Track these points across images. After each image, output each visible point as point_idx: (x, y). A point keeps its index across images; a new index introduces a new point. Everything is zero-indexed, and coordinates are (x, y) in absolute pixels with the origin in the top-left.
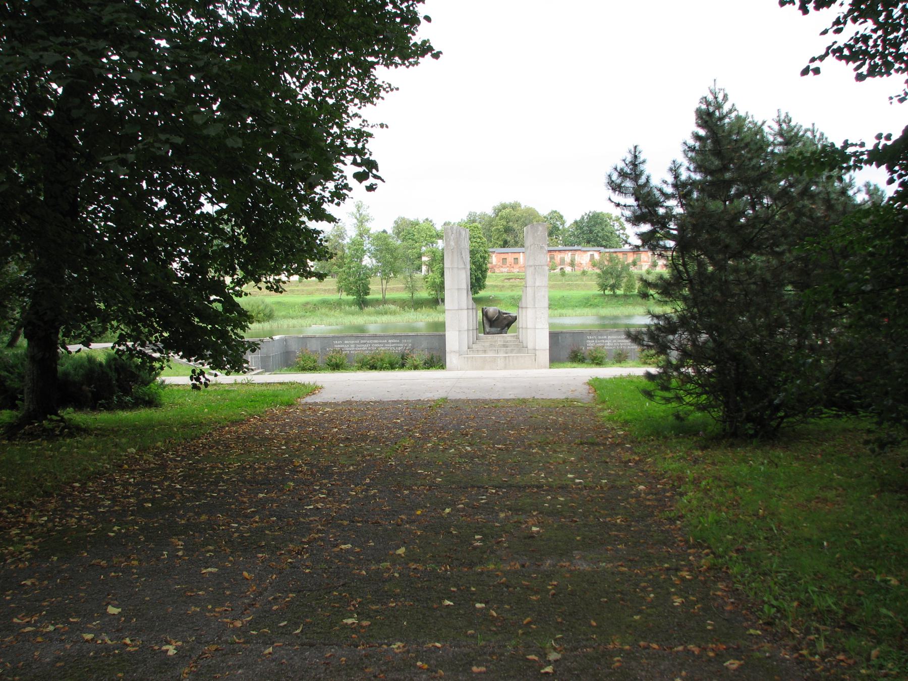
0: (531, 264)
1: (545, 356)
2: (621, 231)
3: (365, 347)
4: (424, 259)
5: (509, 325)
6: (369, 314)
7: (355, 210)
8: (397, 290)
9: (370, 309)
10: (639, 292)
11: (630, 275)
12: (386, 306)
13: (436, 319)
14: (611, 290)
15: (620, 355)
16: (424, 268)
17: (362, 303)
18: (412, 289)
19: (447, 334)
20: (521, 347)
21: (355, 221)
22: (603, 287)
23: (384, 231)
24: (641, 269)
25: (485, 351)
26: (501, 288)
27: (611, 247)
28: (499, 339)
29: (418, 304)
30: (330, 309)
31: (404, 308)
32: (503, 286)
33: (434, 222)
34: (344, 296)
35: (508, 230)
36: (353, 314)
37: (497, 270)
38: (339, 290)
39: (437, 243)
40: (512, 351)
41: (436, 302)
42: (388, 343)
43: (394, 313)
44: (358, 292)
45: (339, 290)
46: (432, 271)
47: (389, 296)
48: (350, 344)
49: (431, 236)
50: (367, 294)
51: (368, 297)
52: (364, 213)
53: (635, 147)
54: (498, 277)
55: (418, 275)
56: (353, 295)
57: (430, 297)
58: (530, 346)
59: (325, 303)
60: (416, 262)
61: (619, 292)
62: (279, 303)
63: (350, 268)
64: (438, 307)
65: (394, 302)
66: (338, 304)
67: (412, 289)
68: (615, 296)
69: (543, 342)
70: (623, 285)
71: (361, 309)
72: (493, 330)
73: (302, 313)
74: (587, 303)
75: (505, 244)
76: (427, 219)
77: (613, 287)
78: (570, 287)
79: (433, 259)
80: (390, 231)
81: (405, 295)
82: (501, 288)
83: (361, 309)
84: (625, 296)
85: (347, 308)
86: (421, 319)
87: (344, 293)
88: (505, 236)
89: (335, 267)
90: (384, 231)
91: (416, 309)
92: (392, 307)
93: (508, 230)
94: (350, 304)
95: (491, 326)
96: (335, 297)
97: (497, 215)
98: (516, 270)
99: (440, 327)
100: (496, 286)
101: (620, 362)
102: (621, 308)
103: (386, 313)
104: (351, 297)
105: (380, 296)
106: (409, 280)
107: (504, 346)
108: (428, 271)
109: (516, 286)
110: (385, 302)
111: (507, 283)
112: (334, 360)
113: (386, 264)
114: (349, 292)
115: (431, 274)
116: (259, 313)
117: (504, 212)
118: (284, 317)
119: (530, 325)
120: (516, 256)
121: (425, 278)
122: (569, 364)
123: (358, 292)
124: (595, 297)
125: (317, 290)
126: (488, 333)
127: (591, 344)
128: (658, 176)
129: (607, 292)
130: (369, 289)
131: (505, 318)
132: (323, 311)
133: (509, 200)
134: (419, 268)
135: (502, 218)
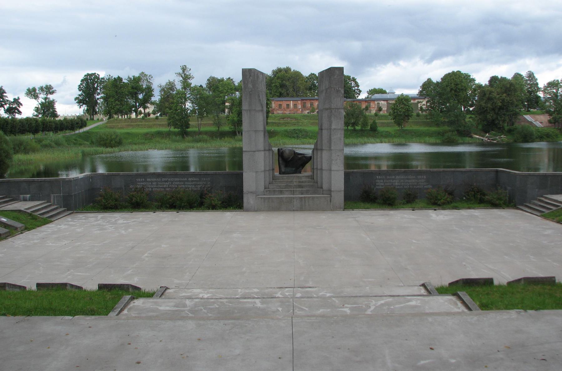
0: (327, 107)
1: (339, 198)
2: (356, 88)
3: (166, 185)
4: (227, 104)
5: (303, 165)
6: (189, 142)
7: (181, 71)
8: (209, 125)
9: (190, 138)
10: (371, 128)
11: (365, 117)
12: (201, 136)
13: (234, 146)
14: (352, 126)
15: (408, 195)
16: (226, 110)
17: (184, 134)
18: (218, 124)
19: (245, 175)
20: (316, 186)
21: (181, 79)
22: (347, 124)
23: (201, 86)
24: (370, 112)
25: (281, 192)
27: (350, 98)
28: (294, 178)
29: (222, 135)
30: (163, 137)
31: (212, 137)
32: (279, 123)
33: (234, 80)
34: (172, 129)
35: (282, 86)
36: (177, 141)
37: (275, 112)
38: (169, 125)
39: (235, 94)
40: (307, 192)
41: (235, 132)
42: (188, 181)
43: (205, 141)
44: (182, 126)
45: (169, 125)
46: (232, 113)
47: (203, 129)
48: (152, 182)
49: (231, 89)
50: (188, 127)
51: (189, 130)
52: (187, 73)
54: (276, 117)
55: (222, 115)
56: (178, 128)
57: (231, 130)
58: (325, 186)
59: (159, 134)
60: (221, 106)
61: (358, 128)
62: (128, 133)
63: (176, 110)
64: (236, 137)
65: (206, 133)
67: (218, 124)
68: (355, 130)
69: (337, 180)
70: (360, 123)
71: (183, 137)
72: (289, 169)
73: (143, 141)
75: (281, 95)
76: (229, 78)
77: (354, 124)
79: (232, 105)
80: (204, 86)
81: (214, 129)
82: (278, 124)
83: (183, 137)
84: (361, 130)
85: (174, 137)
86: (224, 146)
87: (172, 127)
88: (280, 90)
89: (167, 109)
90: (201, 86)
91: (221, 139)
92: (205, 137)
93: (282, 86)
95: (286, 166)
97: (275, 76)
99: (237, 157)
100: (275, 123)
102: (359, 139)
103: (200, 141)
104: (176, 130)
105: (197, 129)
106: (216, 118)
107: (300, 186)
108: (229, 113)
109: (288, 123)
110: (200, 133)
111: (282, 121)
112: (134, 199)
113: (201, 108)
114: (175, 126)
115: (231, 114)
116: (111, 141)
117: (279, 75)
118: (130, 143)
119: (325, 166)
120: (288, 103)
121: (227, 117)
122: (362, 204)
123: (182, 126)
125: (155, 125)
126: (284, 173)
127: (380, 184)
129: (349, 128)
130: (189, 124)
131: (300, 159)
132: (157, 139)
134: (224, 111)
135: (278, 78)
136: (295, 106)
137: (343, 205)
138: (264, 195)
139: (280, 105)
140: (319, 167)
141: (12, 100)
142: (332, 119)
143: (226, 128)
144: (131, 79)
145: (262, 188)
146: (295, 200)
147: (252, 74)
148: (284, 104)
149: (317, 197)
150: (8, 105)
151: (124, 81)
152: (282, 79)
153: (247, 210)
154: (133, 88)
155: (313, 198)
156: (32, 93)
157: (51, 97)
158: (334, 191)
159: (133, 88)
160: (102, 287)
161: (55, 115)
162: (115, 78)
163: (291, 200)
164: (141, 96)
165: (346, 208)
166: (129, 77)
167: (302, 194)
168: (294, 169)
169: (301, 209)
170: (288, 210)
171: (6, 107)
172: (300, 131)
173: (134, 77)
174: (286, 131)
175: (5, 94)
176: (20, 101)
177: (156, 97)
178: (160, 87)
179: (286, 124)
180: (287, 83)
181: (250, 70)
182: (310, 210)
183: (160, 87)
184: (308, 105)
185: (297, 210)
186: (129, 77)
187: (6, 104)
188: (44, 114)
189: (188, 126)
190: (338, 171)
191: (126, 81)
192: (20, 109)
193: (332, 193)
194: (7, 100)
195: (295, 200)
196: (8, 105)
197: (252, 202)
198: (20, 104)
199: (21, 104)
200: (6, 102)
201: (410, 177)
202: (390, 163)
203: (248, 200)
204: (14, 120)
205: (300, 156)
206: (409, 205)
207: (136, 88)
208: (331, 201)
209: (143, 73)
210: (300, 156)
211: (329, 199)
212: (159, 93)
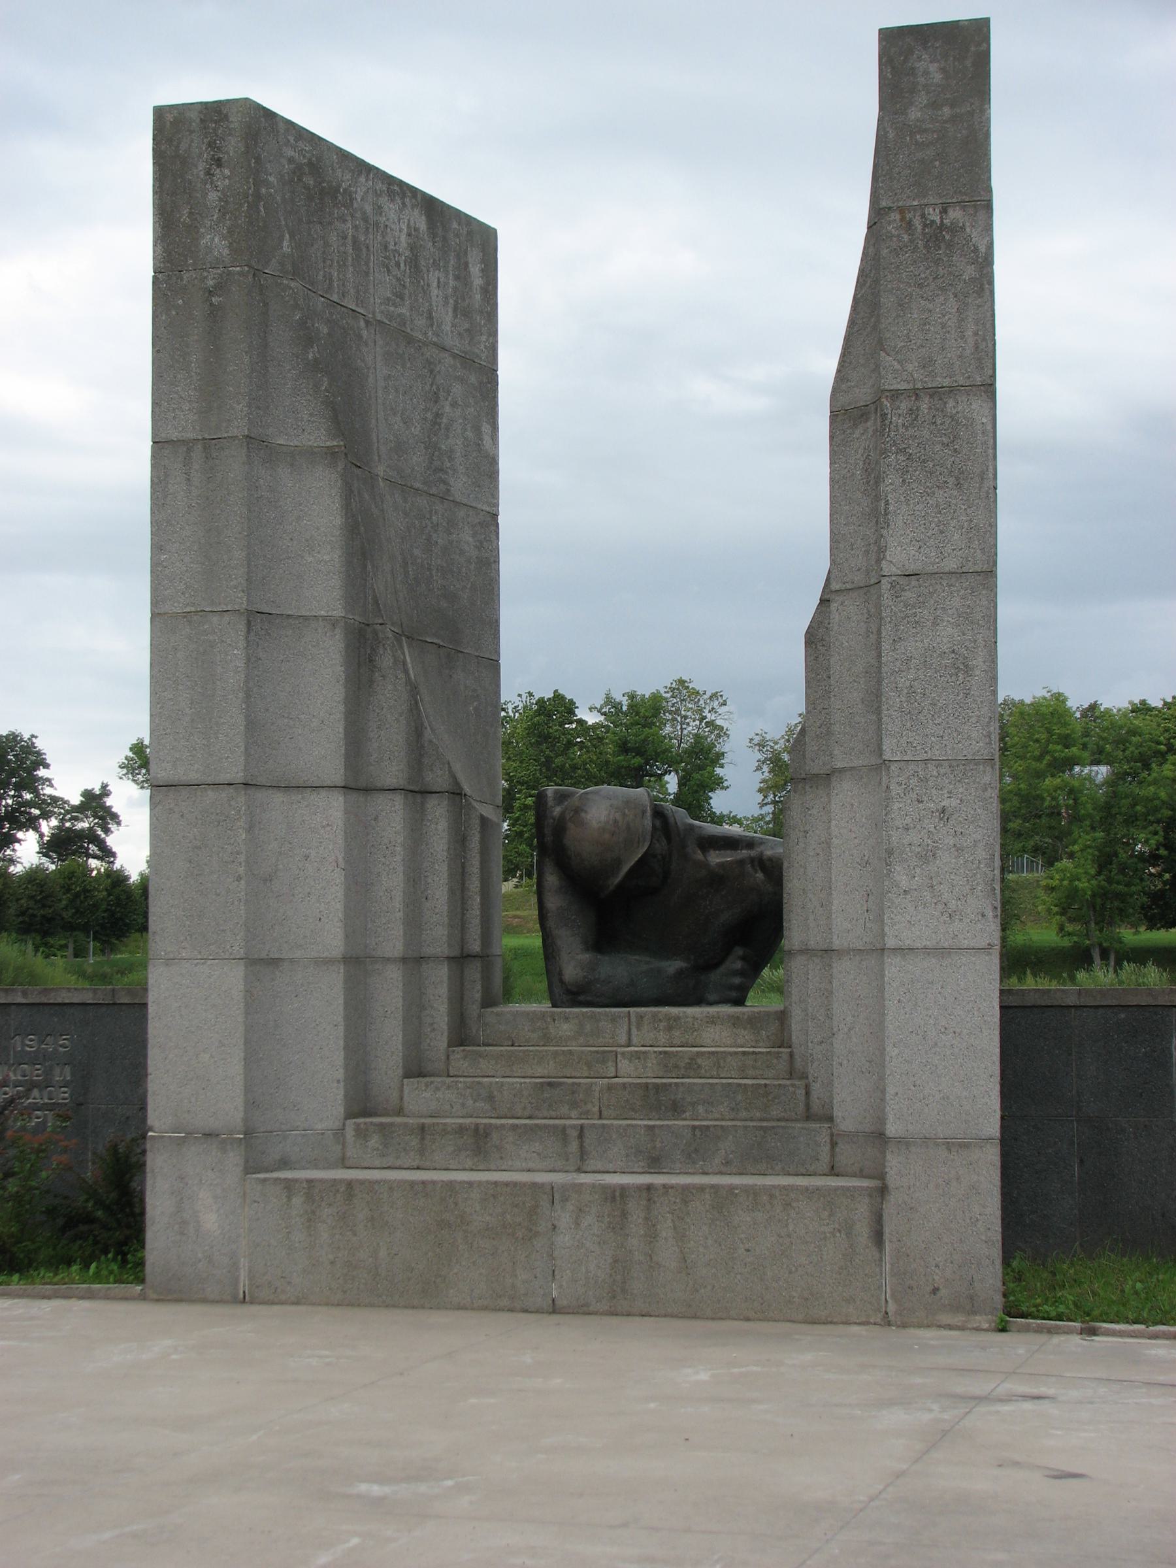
1: (958, 1203)
20: (787, 1114)
28: (640, 1041)
57: (1066, 943)
58: (849, 1113)
72: (618, 968)
95: (603, 939)
131: (717, 879)
137: (990, 1278)
138: (343, 1163)
140: (392, 815)
141: (76, 800)
142: (892, 480)
144: (617, 706)
145: (317, 1095)
146: (564, 1219)
147: (233, 146)
149: (753, 1192)
150: (54, 822)
151: (583, 714)
153: (179, 1292)
154: (624, 747)
155: (723, 1198)
158: (904, 1143)
159: (624, 747)
162: (541, 702)
163: (529, 1210)
165: (1014, 1312)
166: (609, 700)
167: (655, 1163)
168: (673, 966)
169: (619, 1297)
170: (506, 1301)
171: (47, 827)
173: (632, 696)
175: (42, 772)
176: (109, 802)
178: (762, 745)
182: (690, 1312)
183: (762, 745)
185: (581, 1309)
186: (609, 700)
187: (46, 815)
190: (940, 952)
191: (592, 719)
192: (110, 841)
193: (894, 1163)
194: (55, 800)
195: (564, 1219)
196: (54, 822)
197: (210, 1221)
199: (115, 817)
200: (48, 806)
202: (1048, 695)
203: (189, 1202)
205: (716, 858)
207: (639, 752)
208: (878, 1237)
209: (681, 682)
210: (716, 858)
211: (862, 1210)
212: (755, 779)
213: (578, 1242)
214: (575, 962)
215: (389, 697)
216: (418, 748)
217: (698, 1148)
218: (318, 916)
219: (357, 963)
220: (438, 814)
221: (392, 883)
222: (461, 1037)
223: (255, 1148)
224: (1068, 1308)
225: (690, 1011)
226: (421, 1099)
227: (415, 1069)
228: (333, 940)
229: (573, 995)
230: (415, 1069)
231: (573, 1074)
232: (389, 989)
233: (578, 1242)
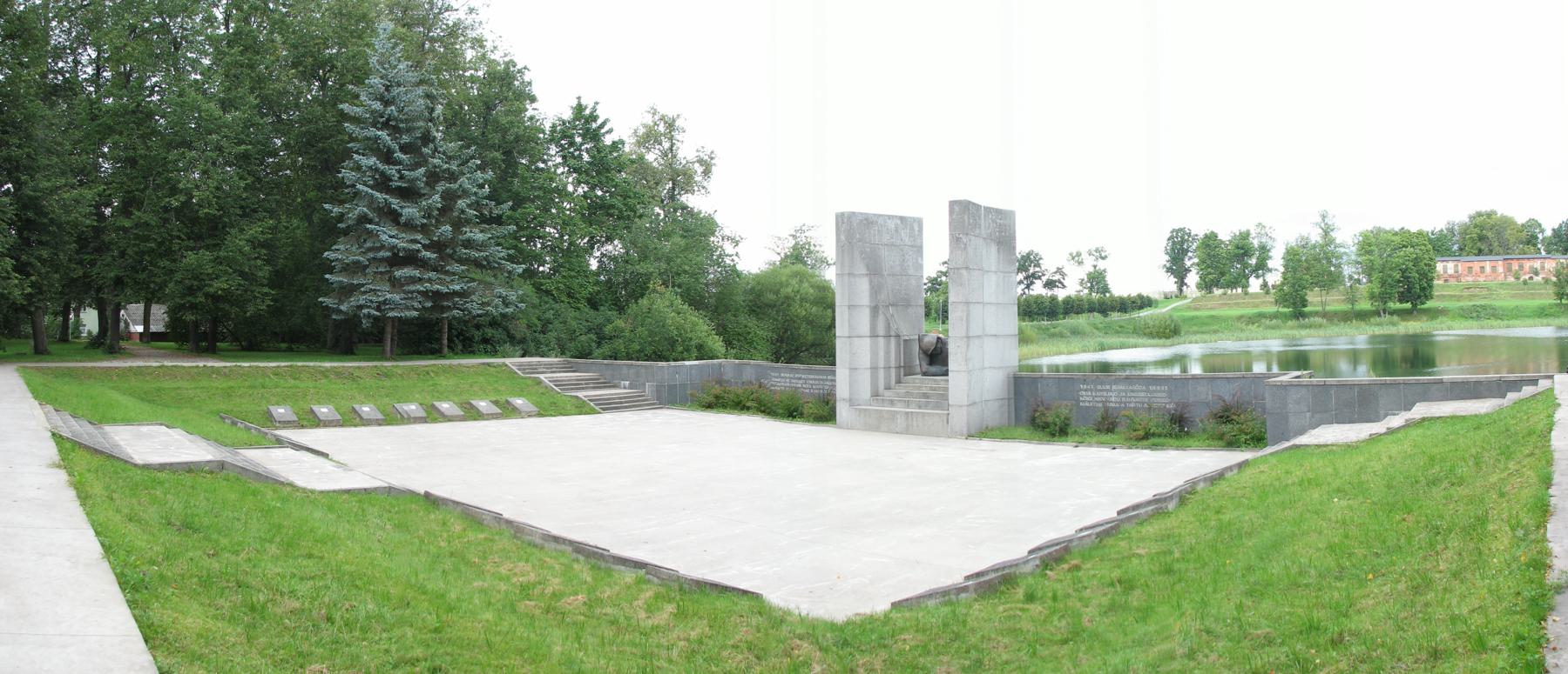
7: (1319, 220)
17: (1299, 315)
18: (1353, 301)
26: (1459, 298)
35: (1482, 238)
53: (1324, 217)
59: (1262, 316)
62: (1213, 317)
66: (1275, 316)
67: (1353, 301)
72: (933, 369)
74: (1542, 313)
75: (1480, 252)
78: (1533, 297)
82: (1459, 298)
92: (1318, 320)
93: (1482, 238)
94: (1285, 317)
96: (1273, 309)
98: (1481, 279)
101: (1227, 409)
105: (1319, 309)
111: (1466, 293)
117: (1479, 220)
124: (1551, 306)
128: (926, 339)
133: (1484, 208)
136: (1494, 268)
139: (1470, 268)
140: (881, 341)
143: (1365, 305)
145: (865, 391)
148: (1476, 266)
152: (1482, 227)
156: (1076, 258)
157: (1101, 265)
160: (896, 605)
161: (1106, 289)
164: (1253, 261)
169: (907, 431)
172: (1484, 307)
174: (1462, 308)
177: (1276, 262)
179: (1471, 297)
180: (1490, 234)
181: (868, 221)
184: (1515, 266)
188: (1091, 289)
189: (1304, 303)
198: (1064, 275)
201: (1137, 387)
203: (842, 410)
204: (1053, 299)
206: (1104, 438)
213: (901, 421)
214: (925, 367)
215: (881, 319)
216: (888, 327)
217: (926, 406)
218: (865, 360)
219: (874, 369)
220: (893, 340)
221: (882, 354)
222: (899, 382)
223: (852, 402)
224: (39, 258)
225: (660, 364)
226: (887, 393)
227: (888, 388)
228: (868, 365)
229: (925, 374)
230: (888, 388)
231: (1415, 433)
232: (881, 374)
233: (901, 421)
